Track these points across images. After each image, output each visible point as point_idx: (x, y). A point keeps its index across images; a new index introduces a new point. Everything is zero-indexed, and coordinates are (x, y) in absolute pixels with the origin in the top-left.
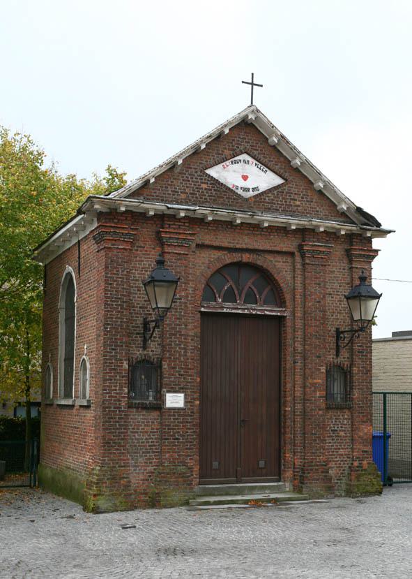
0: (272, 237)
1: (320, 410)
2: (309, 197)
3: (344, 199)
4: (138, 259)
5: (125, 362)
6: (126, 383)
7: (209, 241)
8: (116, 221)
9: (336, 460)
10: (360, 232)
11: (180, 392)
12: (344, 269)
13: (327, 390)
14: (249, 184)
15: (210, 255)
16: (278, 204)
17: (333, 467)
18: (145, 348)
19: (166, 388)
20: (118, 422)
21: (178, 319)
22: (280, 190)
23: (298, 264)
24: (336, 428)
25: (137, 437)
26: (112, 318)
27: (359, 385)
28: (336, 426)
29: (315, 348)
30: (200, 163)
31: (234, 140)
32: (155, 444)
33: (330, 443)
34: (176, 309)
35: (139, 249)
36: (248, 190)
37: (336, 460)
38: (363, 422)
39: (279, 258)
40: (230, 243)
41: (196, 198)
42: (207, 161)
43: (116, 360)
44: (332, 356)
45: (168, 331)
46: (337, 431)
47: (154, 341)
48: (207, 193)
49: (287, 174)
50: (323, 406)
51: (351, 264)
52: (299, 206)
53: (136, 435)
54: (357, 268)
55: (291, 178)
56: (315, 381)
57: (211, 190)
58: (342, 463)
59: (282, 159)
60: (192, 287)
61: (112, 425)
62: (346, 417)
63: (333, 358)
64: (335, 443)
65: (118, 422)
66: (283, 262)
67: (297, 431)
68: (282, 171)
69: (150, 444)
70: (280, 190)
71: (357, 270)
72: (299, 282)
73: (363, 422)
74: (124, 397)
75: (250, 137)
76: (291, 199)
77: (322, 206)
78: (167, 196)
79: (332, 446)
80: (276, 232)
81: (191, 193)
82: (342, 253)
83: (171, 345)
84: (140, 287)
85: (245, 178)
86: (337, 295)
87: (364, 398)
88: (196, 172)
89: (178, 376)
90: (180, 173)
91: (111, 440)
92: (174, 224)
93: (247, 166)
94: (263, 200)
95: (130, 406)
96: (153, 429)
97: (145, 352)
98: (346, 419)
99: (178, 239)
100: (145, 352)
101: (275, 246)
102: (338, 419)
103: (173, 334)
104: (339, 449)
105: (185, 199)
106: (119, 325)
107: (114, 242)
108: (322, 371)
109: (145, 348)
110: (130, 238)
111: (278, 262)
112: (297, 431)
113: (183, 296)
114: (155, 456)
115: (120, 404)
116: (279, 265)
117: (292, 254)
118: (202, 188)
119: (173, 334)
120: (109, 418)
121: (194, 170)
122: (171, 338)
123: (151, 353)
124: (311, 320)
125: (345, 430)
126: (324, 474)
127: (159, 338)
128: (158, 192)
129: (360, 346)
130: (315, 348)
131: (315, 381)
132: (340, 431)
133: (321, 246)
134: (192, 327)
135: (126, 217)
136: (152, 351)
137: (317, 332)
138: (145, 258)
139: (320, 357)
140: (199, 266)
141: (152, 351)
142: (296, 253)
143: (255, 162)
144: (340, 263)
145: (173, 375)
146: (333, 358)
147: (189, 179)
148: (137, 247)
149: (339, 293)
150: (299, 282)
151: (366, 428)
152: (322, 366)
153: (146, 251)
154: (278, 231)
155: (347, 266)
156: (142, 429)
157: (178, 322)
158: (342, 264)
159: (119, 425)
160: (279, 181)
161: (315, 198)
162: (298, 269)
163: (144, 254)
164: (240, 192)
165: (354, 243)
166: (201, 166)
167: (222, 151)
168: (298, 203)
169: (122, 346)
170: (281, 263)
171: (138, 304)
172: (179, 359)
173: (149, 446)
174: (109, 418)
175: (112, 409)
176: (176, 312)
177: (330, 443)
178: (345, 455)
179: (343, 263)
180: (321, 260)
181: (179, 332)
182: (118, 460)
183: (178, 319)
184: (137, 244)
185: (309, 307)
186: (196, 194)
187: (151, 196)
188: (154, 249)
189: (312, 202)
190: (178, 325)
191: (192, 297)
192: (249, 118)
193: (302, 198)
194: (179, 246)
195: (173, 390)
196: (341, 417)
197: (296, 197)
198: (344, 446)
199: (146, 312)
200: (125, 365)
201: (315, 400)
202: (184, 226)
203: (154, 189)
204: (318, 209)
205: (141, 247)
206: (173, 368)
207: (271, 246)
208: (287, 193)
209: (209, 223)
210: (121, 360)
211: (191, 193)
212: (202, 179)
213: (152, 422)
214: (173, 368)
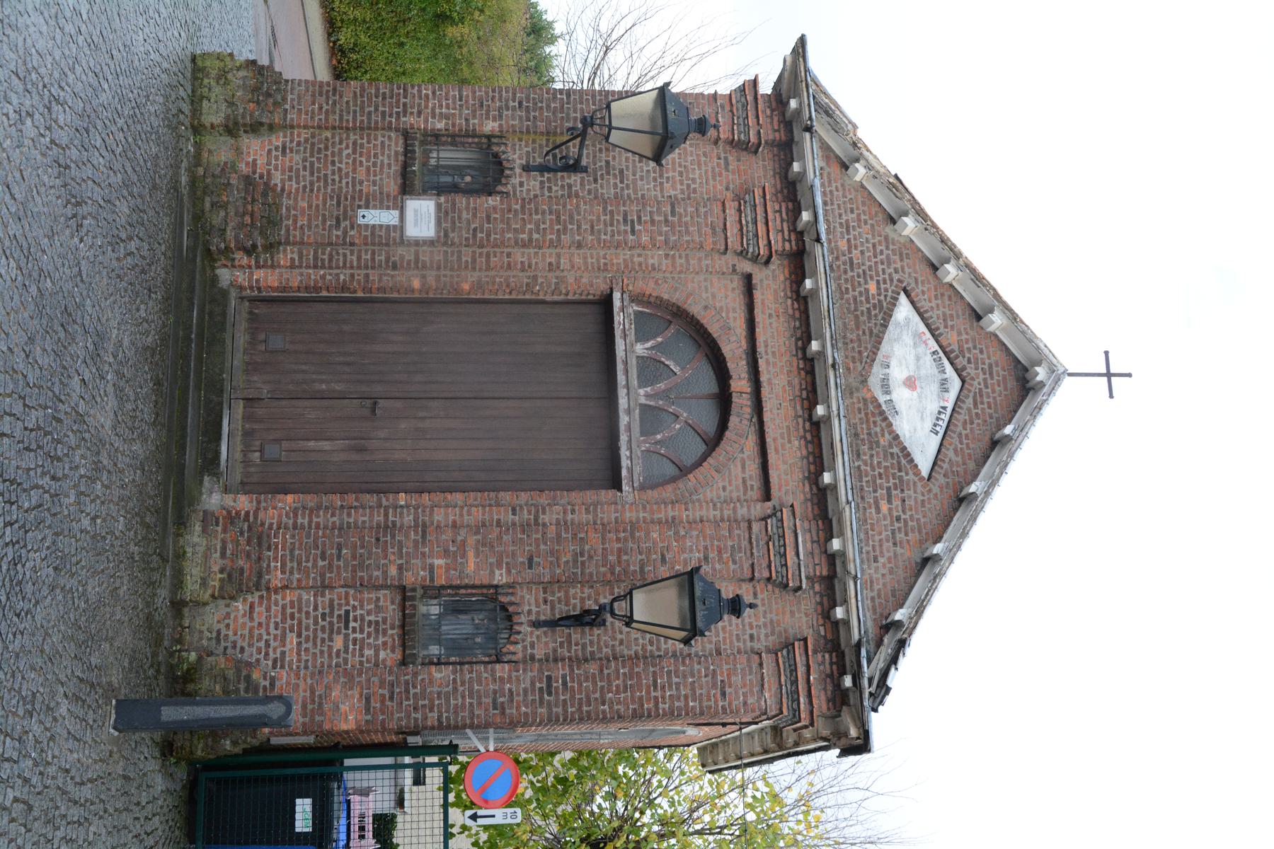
0: (796, 443)
1: (400, 568)
3: (1022, 429)
4: (703, 159)
5: (496, 125)
6: (454, 125)
7: (763, 300)
8: (768, 112)
9: (272, 626)
10: (836, 695)
11: (438, 232)
12: (752, 637)
13: (451, 587)
14: (901, 396)
15: (734, 311)
16: (872, 456)
17: (251, 619)
18: (527, 168)
19: (447, 202)
20: (376, 110)
21: (592, 227)
22: (903, 461)
24: (352, 624)
25: (345, 153)
26: (581, 103)
27: (463, 683)
28: (356, 625)
29: (552, 552)
30: (916, 279)
31: (981, 352)
32: (330, 188)
33: (316, 609)
34: (612, 225)
35: (722, 161)
36: (888, 392)
37: (272, 626)
38: (368, 700)
39: (753, 468)
40: (766, 346)
41: (845, 272)
42: (923, 292)
43: (500, 108)
44: (534, 609)
45: (564, 206)
46: (347, 627)
47: (542, 188)
48: (860, 293)
49: (942, 480)
50: (409, 579)
52: (878, 510)
53: (350, 151)
54: (761, 665)
55: (936, 490)
56: (471, 554)
57: (868, 302)
58: (262, 644)
61: (370, 99)
62: (382, 655)
63: (530, 612)
64: (316, 623)
65: (376, 110)
66: (744, 480)
67: (349, 515)
68: (946, 466)
69: (330, 177)
70: (903, 461)
71: (755, 666)
73: (368, 700)
74: (426, 121)
75: (997, 389)
76: (888, 489)
77: (891, 573)
78: (837, 212)
79: (307, 613)
80: (809, 453)
83: (537, 213)
85: (910, 383)
87: (431, 701)
88: (896, 271)
89: (473, 226)
90: (886, 238)
91: (341, 97)
92: (782, 221)
93: (935, 387)
94: (875, 419)
96: (361, 183)
97: (518, 171)
98: (377, 655)
99: (755, 223)
100: (518, 171)
101: (776, 450)
102: (377, 631)
103: (558, 217)
104: (299, 635)
105: (837, 249)
106: (568, 114)
108: (497, 572)
109: (527, 168)
110: (740, 133)
111: (743, 467)
112: (349, 515)
113: (639, 238)
114: (305, 187)
115: (412, 113)
116: (736, 470)
118: (866, 283)
119: (558, 217)
120: (384, 94)
121: (898, 265)
122: (551, 213)
123: (516, 181)
124: (618, 540)
125: (346, 651)
128: (840, 193)
129: (565, 683)
130: (552, 552)
131: (471, 554)
132: (346, 636)
133: (797, 554)
134: (578, 273)
135: (778, 131)
136: (521, 184)
137: (591, 557)
138: (706, 172)
139: (530, 567)
140: (706, 289)
141: (521, 184)
142: (769, 504)
143: (950, 406)
144: (765, 625)
145: (475, 215)
146: (530, 612)
147: (880, 257)
148: (726, 158)
150: (704, 513)
151: (352, 707)
152: (509, 572)
153: (720, 175)
156: (361, 162)
157: (584, 227)
158: (763, 631)
159: (370, 113)
160: (924, 463)
161: (910, 554)
162: (735, 509)
163: (713, 168)
164: (877, 372)
165: (819, 655)
166: (912, 282)
167: (952, 327)
168: (884, 507)
170: (740, 475)
171: (614, 158)
172: (509, 229)
173: (326, 175)
174: (384, 94)
175: (403, 100)
176: (605, 224)
177: (316, 609)
178: (283, 653)
179: (767, 636)
180: (764, 565)
181: (565, 228)
182: (300, 110)
183: (592, 227)
184: (730, 158)
185: (647, 534)
187: (830, 182)
188: (727, 189)
189: (895, 544)
190: (579, 227)
191: (640, 264)
192: (1037, 369)
193: (898, 519)
194: (741, 230)
195: (442, 215)
196: (381, 640)
197: (897, 503)
198: (307, 650)
200: (490, 126)
201: (423, 554)
202: (784, 240)
203: (842, 185)
204: (881, 560)
205: (727, 164)
206: (488, 217)
207: (775, 440)
208: (901, 478)
210: (501, 117)
212: (885, 282)
214: (488, 217)
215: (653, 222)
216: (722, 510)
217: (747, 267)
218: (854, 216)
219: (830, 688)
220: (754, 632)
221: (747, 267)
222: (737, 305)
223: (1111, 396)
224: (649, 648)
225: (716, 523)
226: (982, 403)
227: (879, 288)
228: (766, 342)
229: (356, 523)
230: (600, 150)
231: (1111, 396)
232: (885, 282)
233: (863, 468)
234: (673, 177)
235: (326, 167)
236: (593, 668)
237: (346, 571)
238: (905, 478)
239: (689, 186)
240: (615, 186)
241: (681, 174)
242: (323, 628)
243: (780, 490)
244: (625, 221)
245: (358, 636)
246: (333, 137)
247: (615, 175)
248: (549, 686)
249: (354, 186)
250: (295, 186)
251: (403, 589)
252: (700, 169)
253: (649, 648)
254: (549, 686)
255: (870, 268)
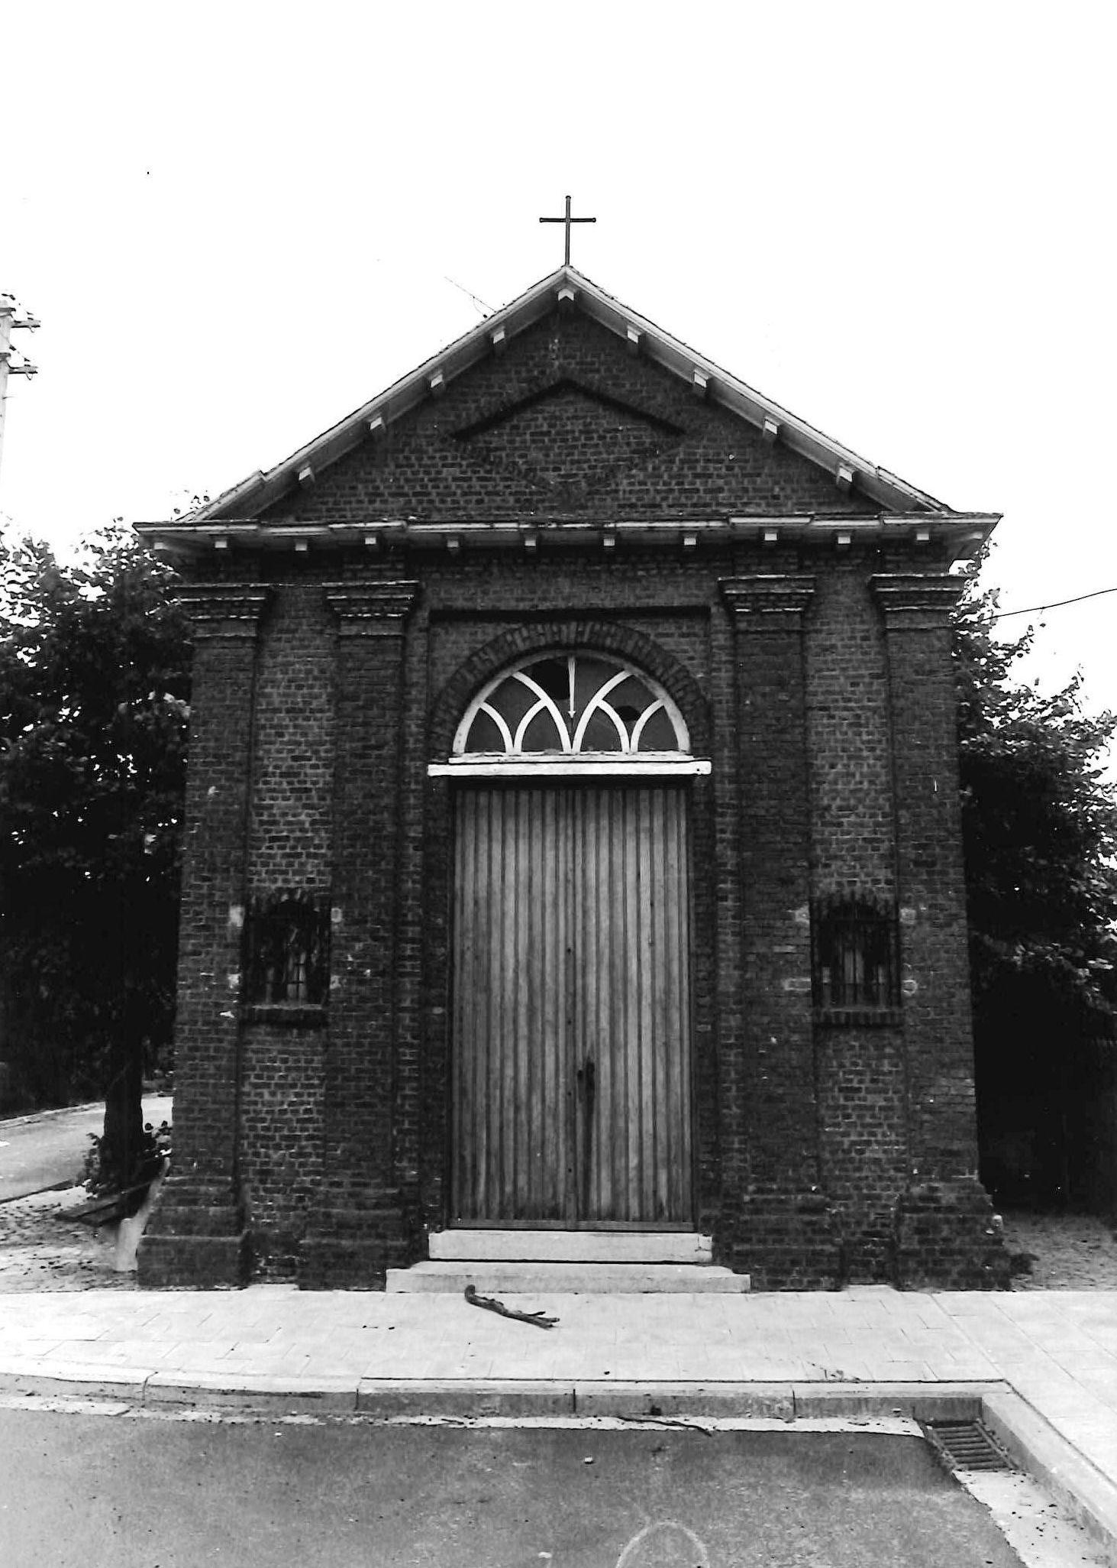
2: (749, 466)
4: (280, 659)
10: (962, 537)
12: (865, 639)
23: (720, 636)
35: (284, 636)
46: (859, 1090)
47: (315, 856)
51: (885, 624)
59: (668, 383)
60: (418, 718)
66: (683, 635)
72: (723, 684)
78: (354, 505)
81: (415, 494)
82: (858, 595)
83: (354, 864)
84: (281, 726)
86: (846, 709)
95: (247, 1022)
107: (214, 625)
110: (251, 613)
111: (667, 635)
116: (669, 644)
117: (700, 613)
126: (807, 1218)
127: (329, 847)
142: (714, 610)
149: (852, 704)
150: (723, 684)
154: (661, 558)
155: (875, 629)
162: (720, 648)
169: (227, 870)
173: (298, 1121)
179: (863, 622)
181: (373, 829)
186: (429, 494)
188: (321, 632)
189: (759, 475)
199: (297, 786)
200: (236, 916)
205: (288, 631)
207: (638, 598)
208: (682, 462)
209: (610, 556)
211: (415, 494)
213: (307, 1061)
215: (365, 724)
216: (720, 662)
217: (423, 615)
218: (360, 486)
219: (924, 558)
220: (859, 635)
221: (423, 615)
222: (468, 630)
223: (593, 220)
224: (878, 752)
225: (737, 668)
226: (593, 363)
227: (452, 465)
228: (518, 600)
229: (737, 1082)
230: (266, 783)
231: (593, 220)
232: (445, 458)
233: (670, 501)
234: (303, 696)
235: (287, 1121)
236: (905, 816)
237: (193, 996)
238: (682, 456)
239: (315, 679)
240: (313, 767)
241: (300, 687)
242: (860, 1117)
243: (697, 596)
244: (362, 756)
245: (868, 1078)
246: (247, 1112)
247: (301, 767)
248: (925, 864)
249: (312, 1086)
250: (313, 1159)
251: (816, 1026)
252: (293, 664)
253: (878, 752)
254: (925, 864)
255: (427, 473)
